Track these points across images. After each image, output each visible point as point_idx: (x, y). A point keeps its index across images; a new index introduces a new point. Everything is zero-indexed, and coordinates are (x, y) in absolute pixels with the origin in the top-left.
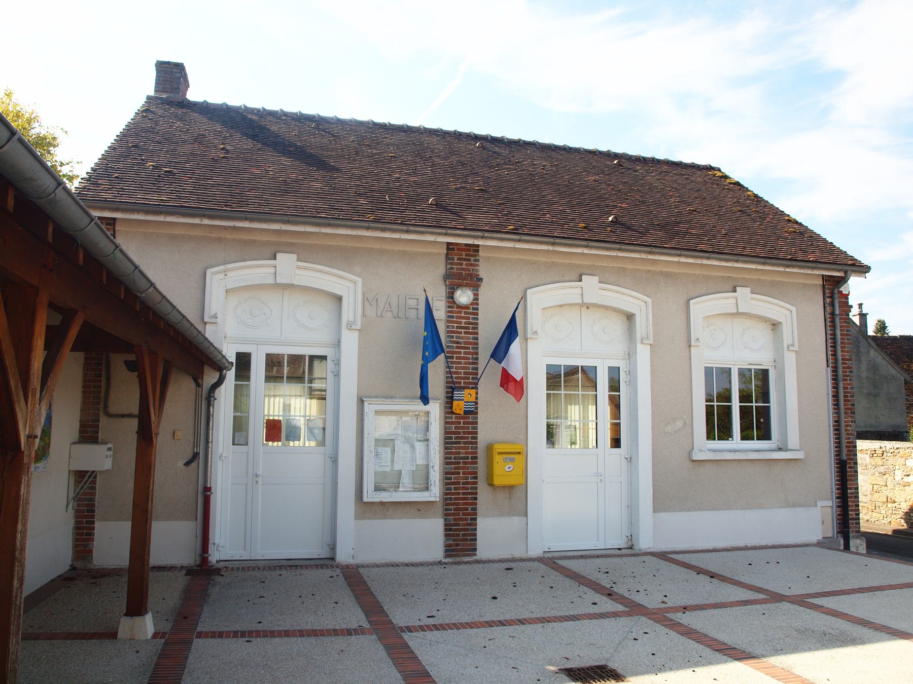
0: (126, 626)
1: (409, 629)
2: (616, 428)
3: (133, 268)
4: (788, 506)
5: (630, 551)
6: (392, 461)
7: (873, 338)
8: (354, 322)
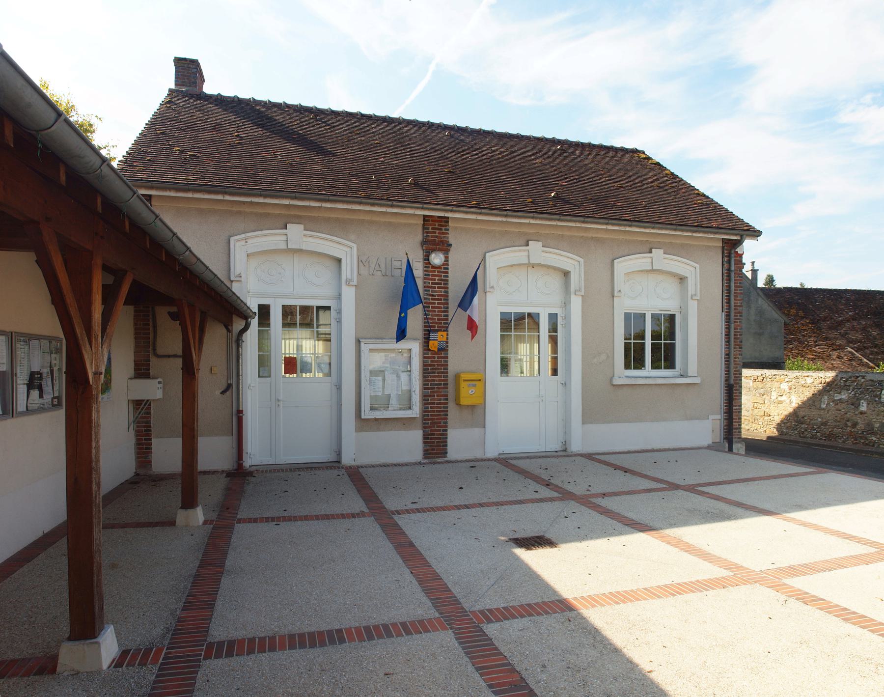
0: (181, 516)
1: (398, 512)
2: (555, 360)
3: (172, 235)
4: (687, 419)
5: (564, 453)
6: (383, 387)
7: (762, 289)
8: (351, 280)
